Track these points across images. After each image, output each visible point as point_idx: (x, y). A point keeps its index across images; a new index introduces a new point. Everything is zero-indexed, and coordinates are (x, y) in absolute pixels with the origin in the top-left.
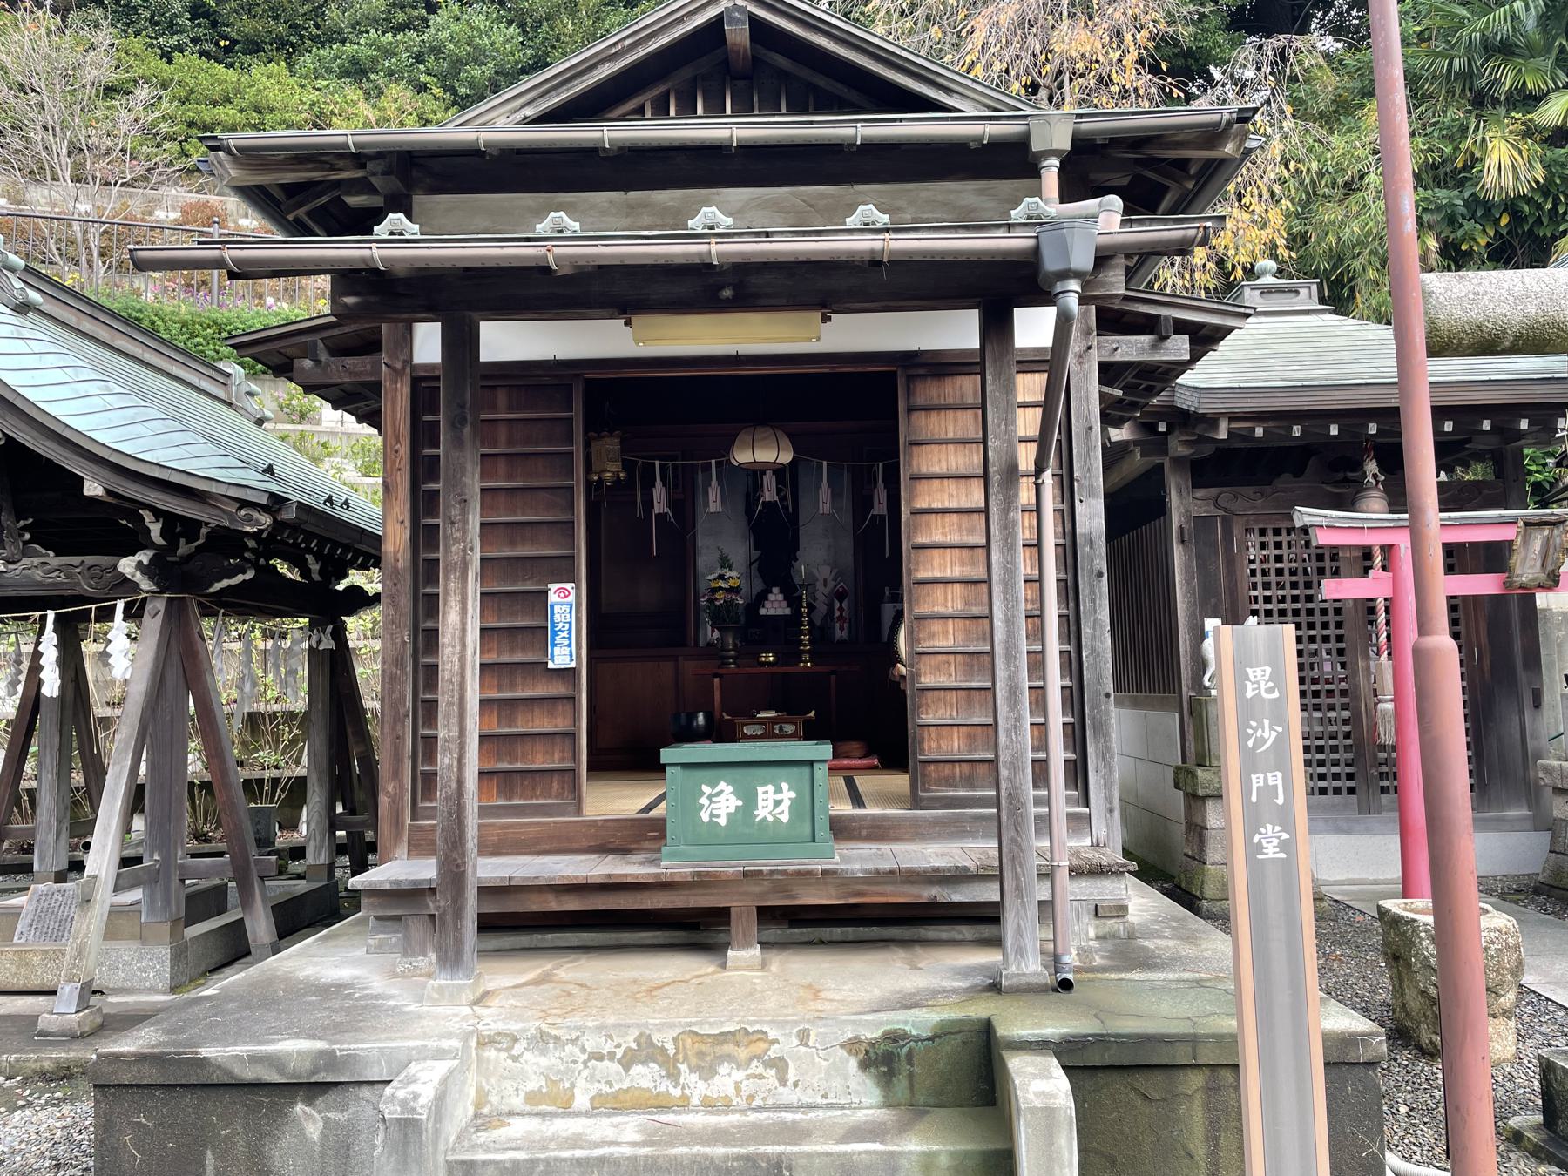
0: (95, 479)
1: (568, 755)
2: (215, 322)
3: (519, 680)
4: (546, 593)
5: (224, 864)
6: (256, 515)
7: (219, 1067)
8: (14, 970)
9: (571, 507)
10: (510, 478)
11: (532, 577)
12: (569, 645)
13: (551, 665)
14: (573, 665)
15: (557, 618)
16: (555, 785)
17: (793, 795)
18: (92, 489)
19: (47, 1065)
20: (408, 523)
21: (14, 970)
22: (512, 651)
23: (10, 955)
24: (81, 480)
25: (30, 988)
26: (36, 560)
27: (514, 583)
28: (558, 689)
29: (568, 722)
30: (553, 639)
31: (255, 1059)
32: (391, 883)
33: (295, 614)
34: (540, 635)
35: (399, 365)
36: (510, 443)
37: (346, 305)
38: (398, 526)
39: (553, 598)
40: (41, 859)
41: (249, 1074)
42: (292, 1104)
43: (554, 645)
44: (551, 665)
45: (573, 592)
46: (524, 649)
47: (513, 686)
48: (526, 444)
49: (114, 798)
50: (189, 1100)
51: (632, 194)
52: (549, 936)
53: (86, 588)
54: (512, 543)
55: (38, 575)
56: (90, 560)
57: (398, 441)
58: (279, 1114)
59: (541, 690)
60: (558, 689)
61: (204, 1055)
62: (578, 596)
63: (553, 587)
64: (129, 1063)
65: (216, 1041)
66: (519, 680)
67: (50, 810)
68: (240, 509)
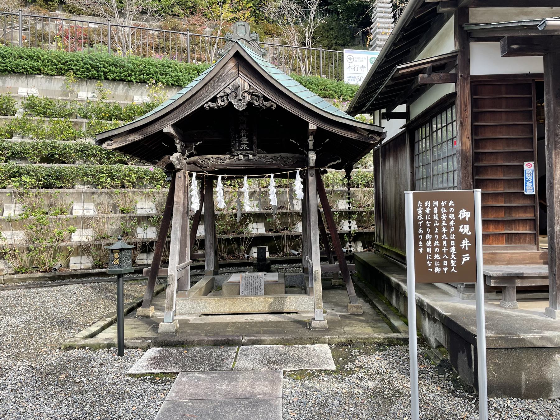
0: (314, 123)
1: (532, 227)
2: (196, 69)
3: (512, 199)
4: (523, 166)
5: (336, 267)
6: (375, 137)
7: (528, 341)
8: (263, 305)
9: (531, 132)
10: (507, 121)
11: (516, 159)
12: (532, 186)
13: (525, 193)
14: (534, 193)
15: (527, 175)
16: (528, 239)
17: (461, 245)
18: (312, 127)
19: (343, 340)
20: (470, 138)
21: (263, 305)
22: (509, 188)
23: (262, 300)
24: (307, 124)
25: (257, 311)
26: (263, 155)
27: (509, 162)
28: (528, 203)
29: (532, 215)
30: (526, 183)
31: (542, 338)
32: (507, 274)
33: (321, 178)
34: (521, 182)
35: (466, 76)
36: (507, 107)
37: (513, 49)
38: (467, 140)
39: (525, 167)
40: (208, 266)
41: (540, 344)
42: (554, 354)
43: (526, 186)
44: (525, 193)
45: (533, 165)
46: (514, 187)
47: (510, 201)
48: (492, 107)
49: (316, 242)
50: (515, 354)
51: (554, 8)
52: (532, 294)
53: (282, 166)
54: (508, 146)
55: (264, 160)
56: (283, 155)
57: (466, 106)
58: (549, 359)
59: (521, 203)
60: (528, 203)
61: (522, 337)
62: (535, 166)
63: (526, 163)
64: (493, 340)
65: (525, 333)
66: (512, 199)
67: (210, 248)
68: (368, 134)
